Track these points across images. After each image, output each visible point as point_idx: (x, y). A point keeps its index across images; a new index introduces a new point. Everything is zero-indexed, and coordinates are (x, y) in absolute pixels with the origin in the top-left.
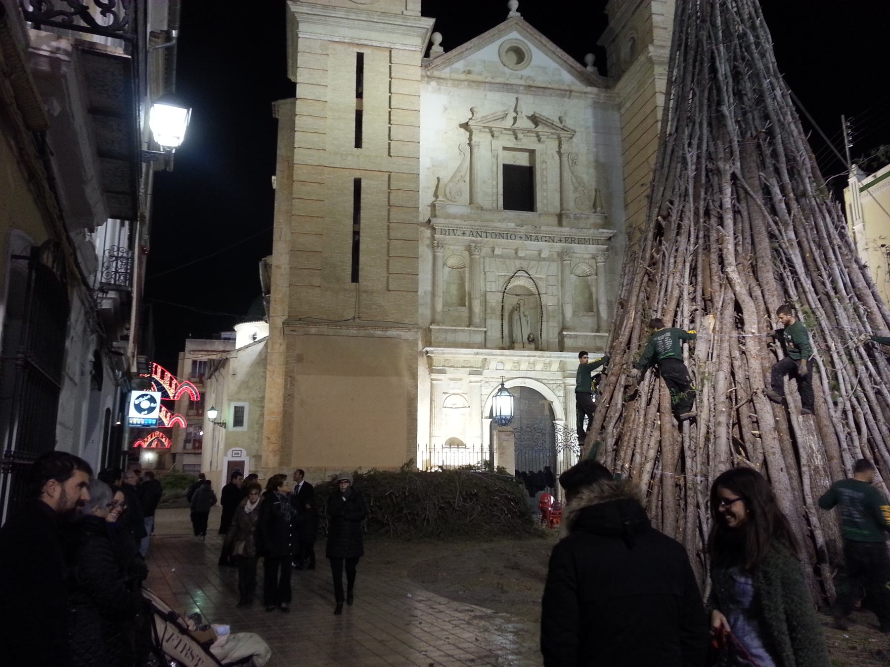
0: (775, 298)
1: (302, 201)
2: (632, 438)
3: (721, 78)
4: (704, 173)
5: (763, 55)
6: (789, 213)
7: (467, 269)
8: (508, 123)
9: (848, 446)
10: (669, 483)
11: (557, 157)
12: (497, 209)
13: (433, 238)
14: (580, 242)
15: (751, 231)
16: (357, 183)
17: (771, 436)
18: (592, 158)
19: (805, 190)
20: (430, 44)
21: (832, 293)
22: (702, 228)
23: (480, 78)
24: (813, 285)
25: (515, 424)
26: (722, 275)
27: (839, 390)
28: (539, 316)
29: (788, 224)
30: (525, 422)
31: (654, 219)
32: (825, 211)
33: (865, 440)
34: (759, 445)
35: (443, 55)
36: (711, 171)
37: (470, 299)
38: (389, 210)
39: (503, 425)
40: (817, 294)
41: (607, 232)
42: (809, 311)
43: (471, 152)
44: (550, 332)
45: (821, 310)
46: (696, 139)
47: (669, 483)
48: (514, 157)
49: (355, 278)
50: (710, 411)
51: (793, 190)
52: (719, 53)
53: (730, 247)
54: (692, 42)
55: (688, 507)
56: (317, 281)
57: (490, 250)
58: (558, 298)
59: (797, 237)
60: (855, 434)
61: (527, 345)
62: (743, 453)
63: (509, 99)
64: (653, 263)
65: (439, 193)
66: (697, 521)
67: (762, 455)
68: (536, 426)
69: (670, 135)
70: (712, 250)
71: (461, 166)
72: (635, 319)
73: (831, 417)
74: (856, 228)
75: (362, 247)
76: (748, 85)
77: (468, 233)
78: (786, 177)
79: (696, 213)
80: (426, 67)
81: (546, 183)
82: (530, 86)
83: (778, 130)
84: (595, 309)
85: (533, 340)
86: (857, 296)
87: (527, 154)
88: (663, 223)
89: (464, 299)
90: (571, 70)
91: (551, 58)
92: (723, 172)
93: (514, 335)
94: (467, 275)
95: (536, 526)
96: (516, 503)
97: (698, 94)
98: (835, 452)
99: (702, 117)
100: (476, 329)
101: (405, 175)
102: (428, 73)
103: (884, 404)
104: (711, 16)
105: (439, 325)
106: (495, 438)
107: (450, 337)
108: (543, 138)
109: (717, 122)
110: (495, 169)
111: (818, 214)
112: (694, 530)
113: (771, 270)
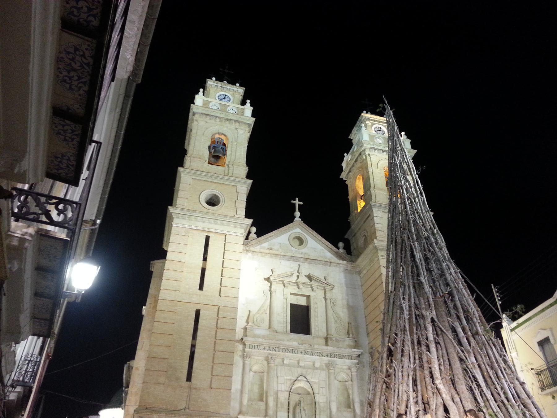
1: (160, 323)
3: (418, 261)
4: (414, 317)
6: (470, 345)
7: (265, 374)
8: (294, 279)
11: (323, 301)
14: (340, 357)
16: (198, 313)
18: (345, 302)
19: (477, 330)
20: (249, 233)
21: (506, 401)
22: (417, 353)
23: (277, 253)
26: (433, 386)
28: (314, 411)
31: (387, 344)
32: (492, 345)
36: (418, 316)
38: (216, 331)
40: (496, 401)
41: (357, 351)
43: (271, 295)
46: (407, 295)
48: (297, 299)
49: (189, 378)
51: (470, 330)
52: (415, 247)
53: (436, 366)
54: (399, 240)
56: (162, 380)
57: (281, 360)
63: (295, 265)
65: (249, 320)
69: (391, 292)
70: (425, 368)
71: (264, 303)
75: (196, 356)
76: (434, 265)
77: (267, 348)
78: (464, 322)
79: (412, 343)
80: (246, 245)
81: (317, 317)
82: (307, 258)
83: (455, 293)
84: (352, 407)
86: (522, 404)
87: (305, 298)
88: (392, 348)
89: (262, 397)
90: (331, 250)
94: (265, 378)
99: (410, 283)
102: (247, 248)
108: (315, 289)
109: (418, 286)
110: (285, 306)
111: (488, 347)
113: (464, 383)
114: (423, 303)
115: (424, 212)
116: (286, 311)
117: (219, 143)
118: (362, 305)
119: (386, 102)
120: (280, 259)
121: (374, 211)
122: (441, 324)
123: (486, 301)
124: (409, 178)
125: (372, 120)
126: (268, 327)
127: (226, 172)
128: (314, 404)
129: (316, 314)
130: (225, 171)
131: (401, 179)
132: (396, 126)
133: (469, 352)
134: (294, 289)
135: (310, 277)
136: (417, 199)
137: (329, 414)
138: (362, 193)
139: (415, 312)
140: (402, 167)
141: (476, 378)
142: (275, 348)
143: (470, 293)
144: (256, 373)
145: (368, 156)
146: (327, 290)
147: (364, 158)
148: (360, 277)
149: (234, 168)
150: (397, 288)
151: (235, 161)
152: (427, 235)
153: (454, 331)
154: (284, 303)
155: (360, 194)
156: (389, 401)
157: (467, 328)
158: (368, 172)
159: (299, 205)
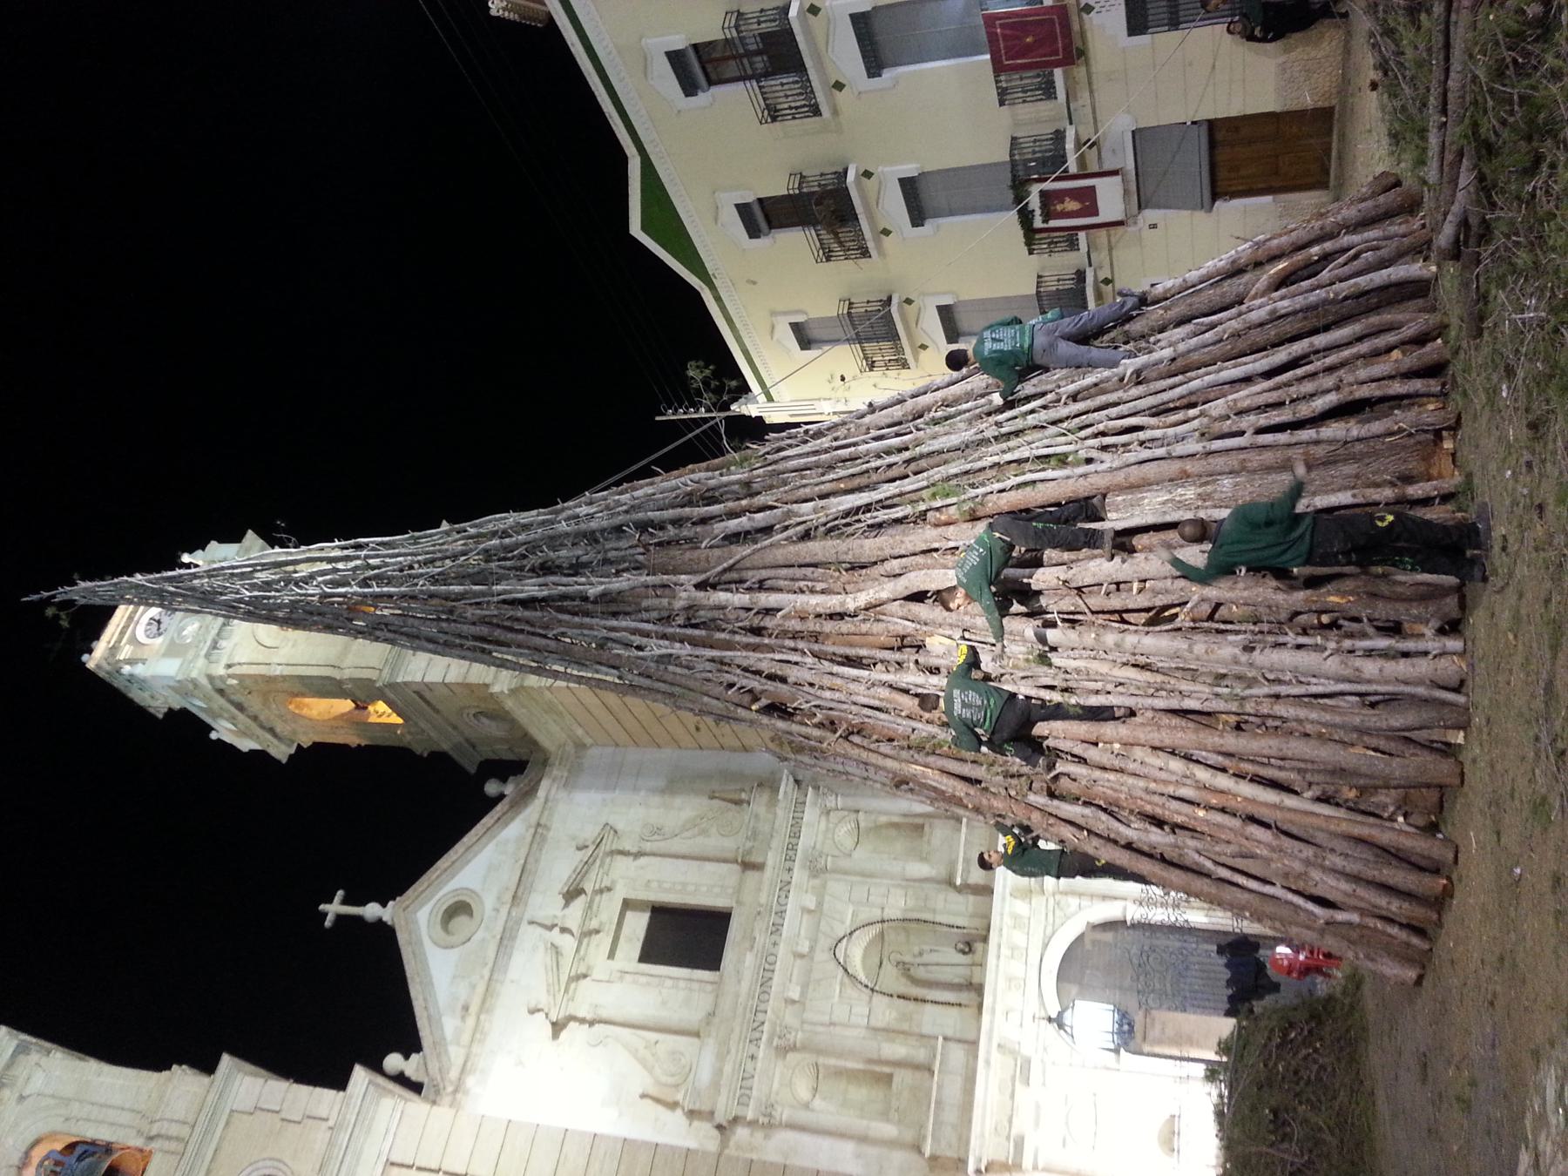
0: (906, 539)
2: (1148, 797)
3: (545, 593)
4: (689, 631)
5: (526, 527)
6: (772, 508)
7: (821, 1060)
8: (567, 943)
9: (1162, 446)
10: (1232, 742)
11: (643, 860)
12: (718, 984)
13: (753, 1124)
14: (796, 835)
15: (793, 566)
17: (1142, 565)
18: (656, 800)
19: (738, 482)
20: (401, 1079)
21: (906, 455)
22: (779, 642)
23: (481, 988)
24: (893, 480)
25: (1131, 1003)
26: (860, 617)
27: (1066, 455)
28: (922, 926)
29: (789, 511)
30: (1127, 982)
31: (754, 716)
32: (776, 456)
33: (1153, 421)
34: (1160, 585)
35: (425, 1058)
36: (689, 619)
37: (880, 1062)
39: (1131, 1030)
40: (907, 476)
41: (786, 786)
42: (932, 489)
44: (955, 910)
45: (931, 472)
46: (633, 638)
47: (1232, 742)
48: (630, 940)
50: (1095, 659)
51: (738, 499)
52: (505, 592)
53: (814, 602)
54: (484, 630)
55: (1278, 714)
58: (894, 886)
59: (812, 500)
60: (1142, 435)
61: (977, 957)
62: (1173, 611)
63: (529, 937)
64: (831, 725)
65: (670, 1099)
66: (1306, 700)
67: (1176, 581)
68: (1135, 961)
69: (620, 678)
70: (818, 628)
72: (926, 766)
73: (1112, 470)
74: (826, 410)
76: (563, 553)
77: (753, 1049)
78: (715, 509)
79: (755, 648)
80: (437, 1092)
81: (684, 885)
82: (514, 897)
83: (641, 515)
84: (919, 821)
85: (968, 944)
86: (914, 419)
87: (629, 915)
88: (764, 702)
89: (879, 1076)
90: (502, 821)
91: (475, 855)
92: (691, 603)
93: (956, 980)
94: (832, 1061)
95: (1339, 989)
96: (1292, 1025)
97: (563, 630)
98: (1174, 467)
99: (601, 626)
100: (938, 1057)
101: (622, 1167)
102: (450, 1089)
103: (1092, 390)
104: (446, 599)
105: (924, 1137)
106: (1158, 1050)
107: (951, 1116)
108: (607, 882)
109: (612, 604)
110: (643, 979)
111: (780, 467)
112: (1325, 708)
113: (859, 541)
114: (656, 602)
115: (412, 549)
116: (657, 980)
117: (58, 1169)
118: (668, 753)
119: (46, 594)
120: (502, 983)
121: (408, 679)
122: (714, 567)
123: (690, 435)
124: (304, 570)
125: (119, 640)
126: (695, 1040)
127: (173, 1146)
128: (905, 924)
129: (679, 887)
130: (167, 1152)
131: (301, 595)
132: (130, 579)
133: (789, 514)
134: (598, 945)
135: (572, 894)
136: (371, 561)
137: (935, 886)
138: (347, 705)
139: (679, 626)
140: (267, 585)
141: (852, 509)
142: (756, 1024)
143: (648, 480)
144: (816, 1090)
145: (231, 671)
146: (614, 848)
147: (235, 682)
148: (592, 745)
149: (168, 1115)
150: (611, 662)
151: (139, 1112)
152: (478, 554)
153: (735, 538)
154: (635, 982)
155: (350, 712)
156: (891, 734)
157: (730, 504)
158: (284, 678)
159: (345, 902)
